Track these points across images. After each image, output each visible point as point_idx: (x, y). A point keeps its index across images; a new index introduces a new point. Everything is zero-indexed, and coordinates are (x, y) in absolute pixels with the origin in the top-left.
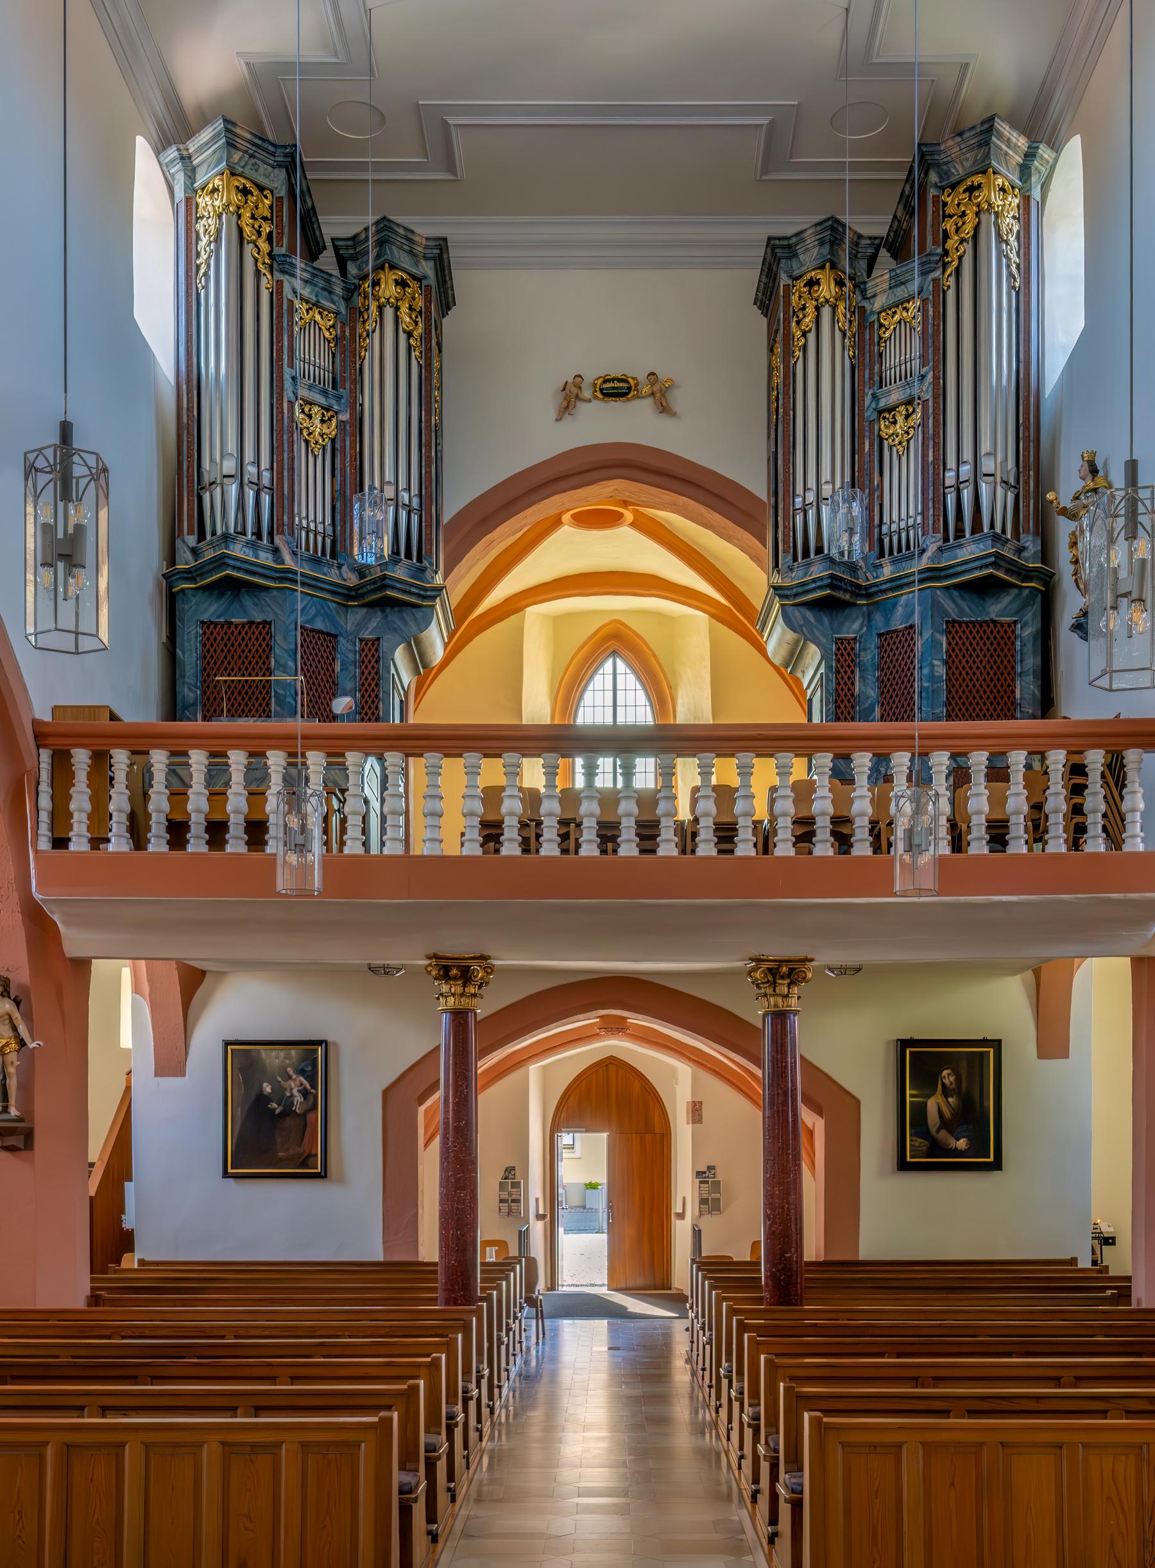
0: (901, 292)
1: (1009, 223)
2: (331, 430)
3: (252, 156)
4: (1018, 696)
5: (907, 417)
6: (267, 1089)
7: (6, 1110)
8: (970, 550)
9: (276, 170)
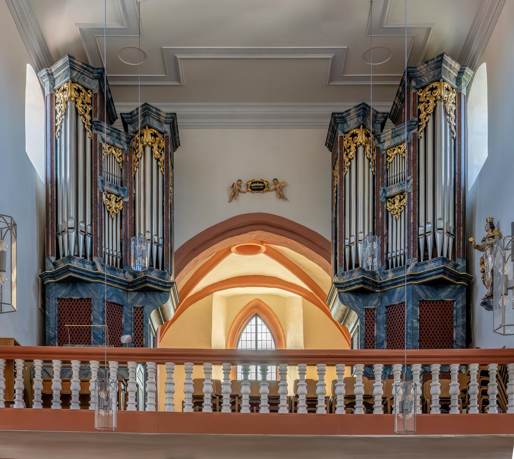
0: (397, 140)
1: (451, 106)
2: (120, 206)
3: (82, 74)
4: (454, 337)
8: (432, 266)
9: (94, 81)
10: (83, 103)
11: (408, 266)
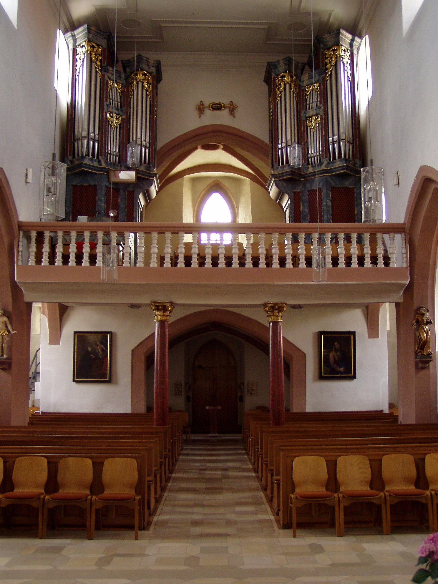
1: (347, 61)
2: (120, 121)
4: (356, 212)
5: (316, 119)
6: (90, 349)
7: (2, 355)
8: (338, 164)
10: (95, 55)
11: (322, 163)
